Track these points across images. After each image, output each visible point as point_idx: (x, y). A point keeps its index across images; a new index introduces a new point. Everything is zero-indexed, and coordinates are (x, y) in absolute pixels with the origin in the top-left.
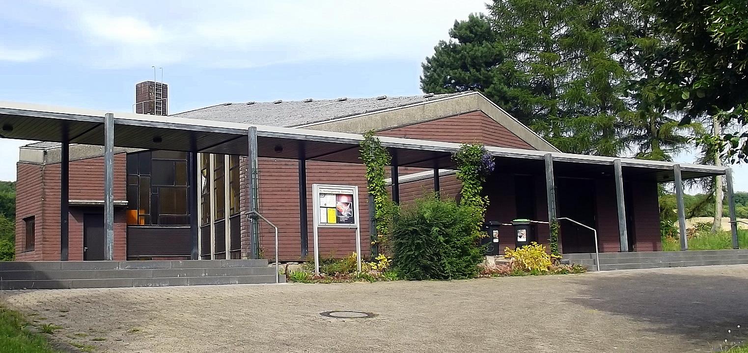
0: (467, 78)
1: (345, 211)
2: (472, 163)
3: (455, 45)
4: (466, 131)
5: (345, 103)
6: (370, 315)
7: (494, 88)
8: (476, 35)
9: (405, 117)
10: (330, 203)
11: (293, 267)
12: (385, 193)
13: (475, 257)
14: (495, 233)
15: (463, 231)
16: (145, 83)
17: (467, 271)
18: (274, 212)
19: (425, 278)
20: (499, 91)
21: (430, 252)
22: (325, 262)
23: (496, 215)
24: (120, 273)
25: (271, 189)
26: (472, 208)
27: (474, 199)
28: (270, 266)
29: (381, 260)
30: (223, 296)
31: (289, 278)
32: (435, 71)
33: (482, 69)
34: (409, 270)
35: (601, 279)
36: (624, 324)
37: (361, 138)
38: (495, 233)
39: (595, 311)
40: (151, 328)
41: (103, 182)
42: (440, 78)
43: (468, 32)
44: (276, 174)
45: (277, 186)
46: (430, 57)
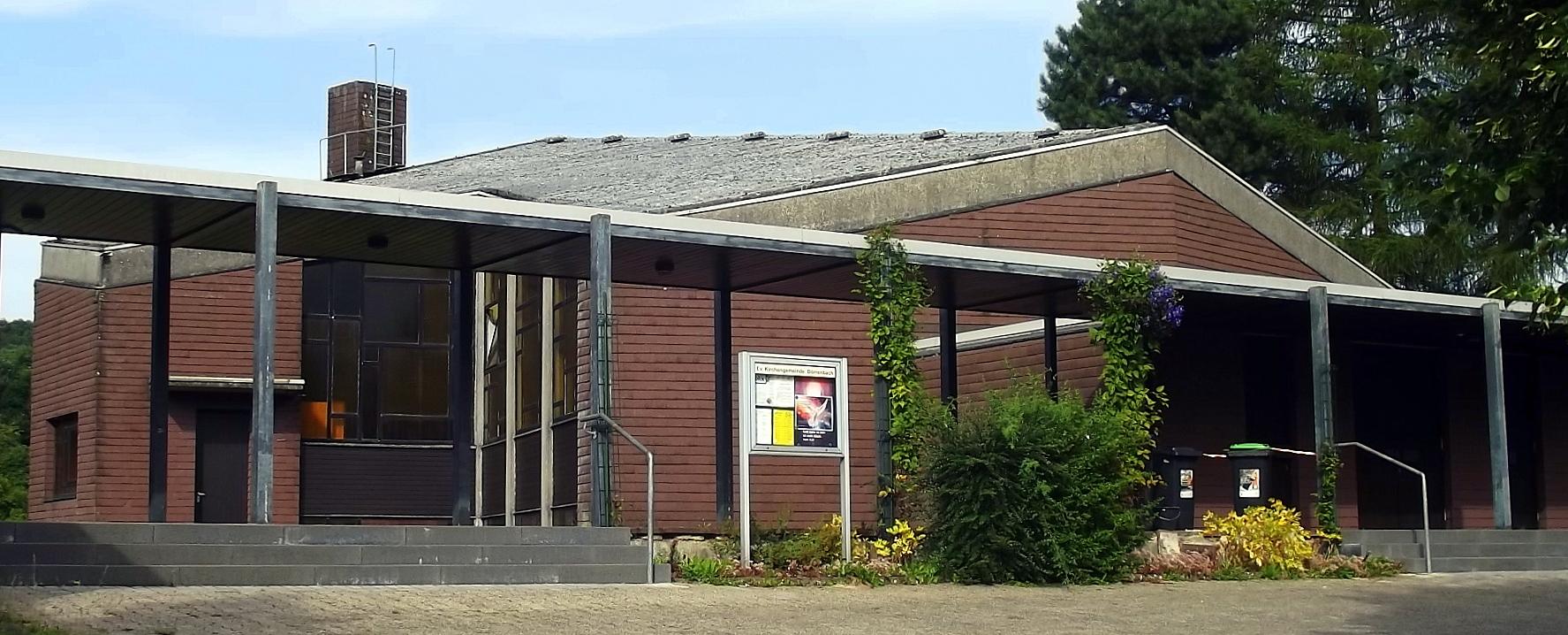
0: (1157, 83)
1: (816, 416)
2: (1128, 308)
5: (843, 148)
10: (780, 399)
11: (689, 547)
12: (914, 375)
14: (1186, 476)
15: (1099, 469)
16: (351, 86)
17: (1106, 565)
18: (660, 414)
19: (1000, 579)
20: (1238, 119)
21: (1015, 516)
23: (1178, 435)
24: (287, 553)
25: (652, 358)
26: (1124, 416)
27: (1131, 394)
28: (637, 542)
29: (899, 535)
30: (521, 610)
31: (678, 572)
32: (1076, 64)
33: (1197, 62)
35: (1427, 591)
37: (858, 242)
38: (1186, 476)
44: (666, 321)
45: (667, 349)
46: (1068, 28)
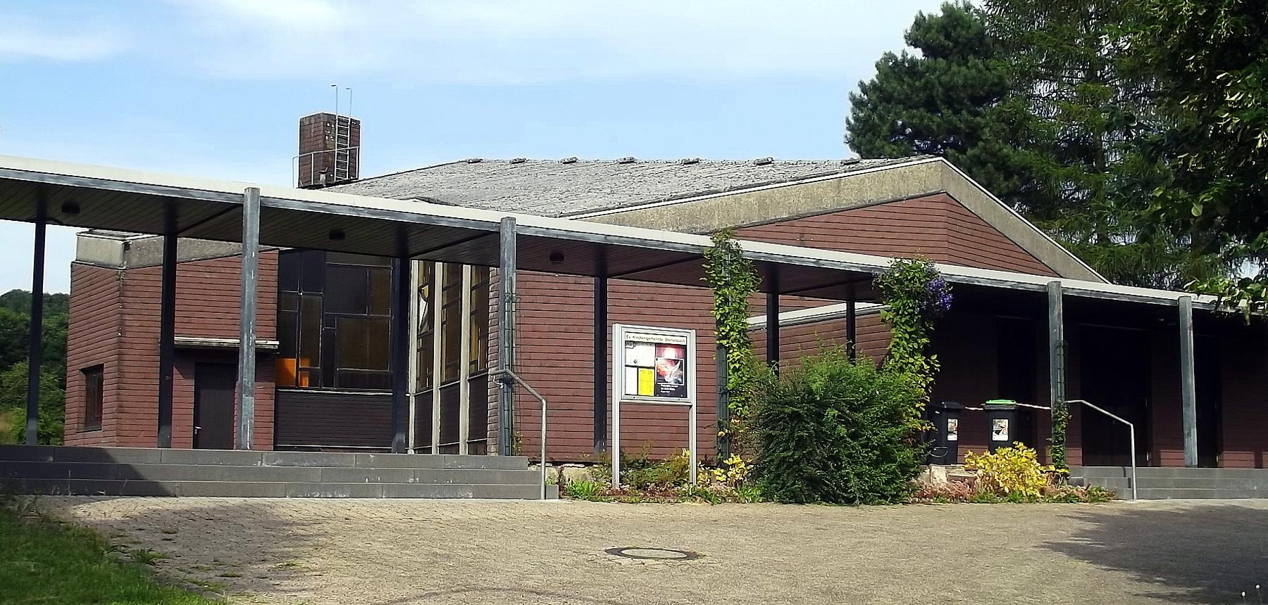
0: (934, 127)
1: (671, 374)
2: (910, 295)
3: (913, 62)
4: (918, 230)
5: (694, 170)
6: (690, 556)
7: (984, 148)
8: (956, 43)
9: (803, 201)
10: (644, 360)
11: (572, 473)
13: (906, 465)
14: (952, 424)
15: (886, 418)
17: (890, 490)
19: (811, 500)
20: (994, 155)
22: (631, 465)
23: (951, 391)
24: (264, 473)
25: (546, 328)
26: (906, 377)
27: (911, 360)
28: (533, 468)
29: (733, 465)
31: (564, 490)
32: (874, 109)
34: (784, 485)
36: (1122, 583)
37: (706, 241)
38: (952, 424)
39: (1083, 565)
40: (317, 563)
41: (237, 310)
42: (884, 124)
43: (942, 38)
46: (867, 82)
